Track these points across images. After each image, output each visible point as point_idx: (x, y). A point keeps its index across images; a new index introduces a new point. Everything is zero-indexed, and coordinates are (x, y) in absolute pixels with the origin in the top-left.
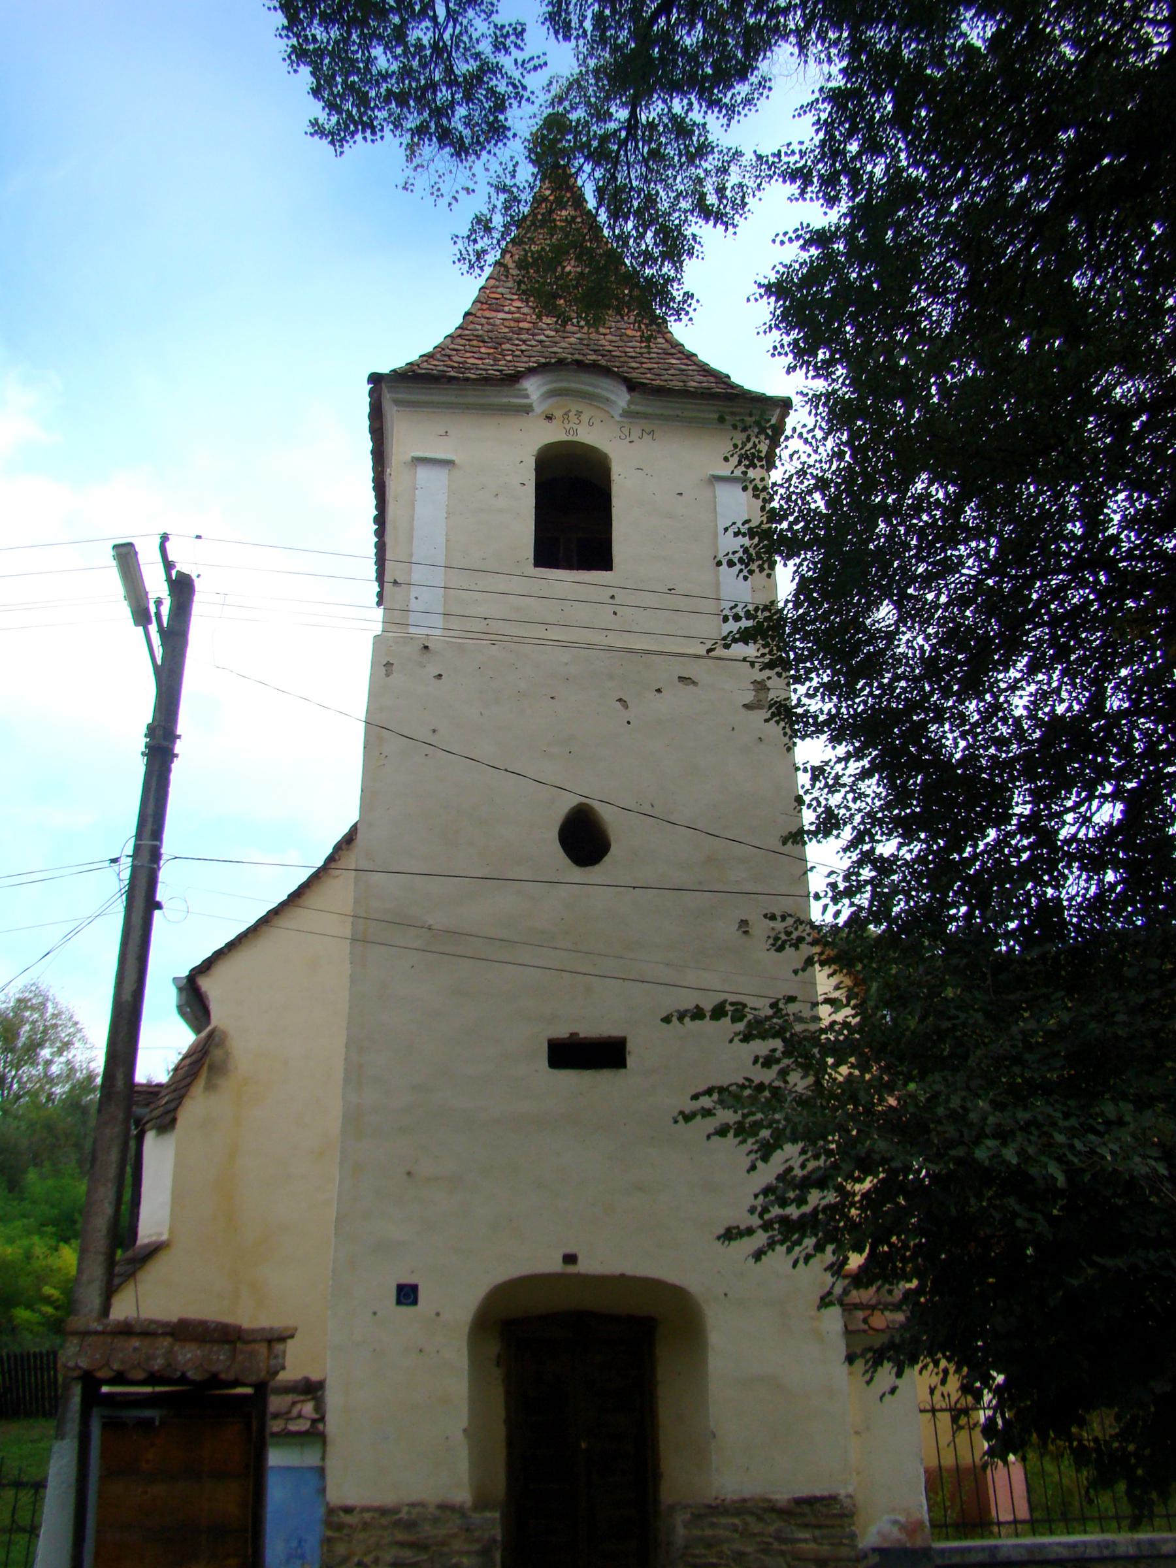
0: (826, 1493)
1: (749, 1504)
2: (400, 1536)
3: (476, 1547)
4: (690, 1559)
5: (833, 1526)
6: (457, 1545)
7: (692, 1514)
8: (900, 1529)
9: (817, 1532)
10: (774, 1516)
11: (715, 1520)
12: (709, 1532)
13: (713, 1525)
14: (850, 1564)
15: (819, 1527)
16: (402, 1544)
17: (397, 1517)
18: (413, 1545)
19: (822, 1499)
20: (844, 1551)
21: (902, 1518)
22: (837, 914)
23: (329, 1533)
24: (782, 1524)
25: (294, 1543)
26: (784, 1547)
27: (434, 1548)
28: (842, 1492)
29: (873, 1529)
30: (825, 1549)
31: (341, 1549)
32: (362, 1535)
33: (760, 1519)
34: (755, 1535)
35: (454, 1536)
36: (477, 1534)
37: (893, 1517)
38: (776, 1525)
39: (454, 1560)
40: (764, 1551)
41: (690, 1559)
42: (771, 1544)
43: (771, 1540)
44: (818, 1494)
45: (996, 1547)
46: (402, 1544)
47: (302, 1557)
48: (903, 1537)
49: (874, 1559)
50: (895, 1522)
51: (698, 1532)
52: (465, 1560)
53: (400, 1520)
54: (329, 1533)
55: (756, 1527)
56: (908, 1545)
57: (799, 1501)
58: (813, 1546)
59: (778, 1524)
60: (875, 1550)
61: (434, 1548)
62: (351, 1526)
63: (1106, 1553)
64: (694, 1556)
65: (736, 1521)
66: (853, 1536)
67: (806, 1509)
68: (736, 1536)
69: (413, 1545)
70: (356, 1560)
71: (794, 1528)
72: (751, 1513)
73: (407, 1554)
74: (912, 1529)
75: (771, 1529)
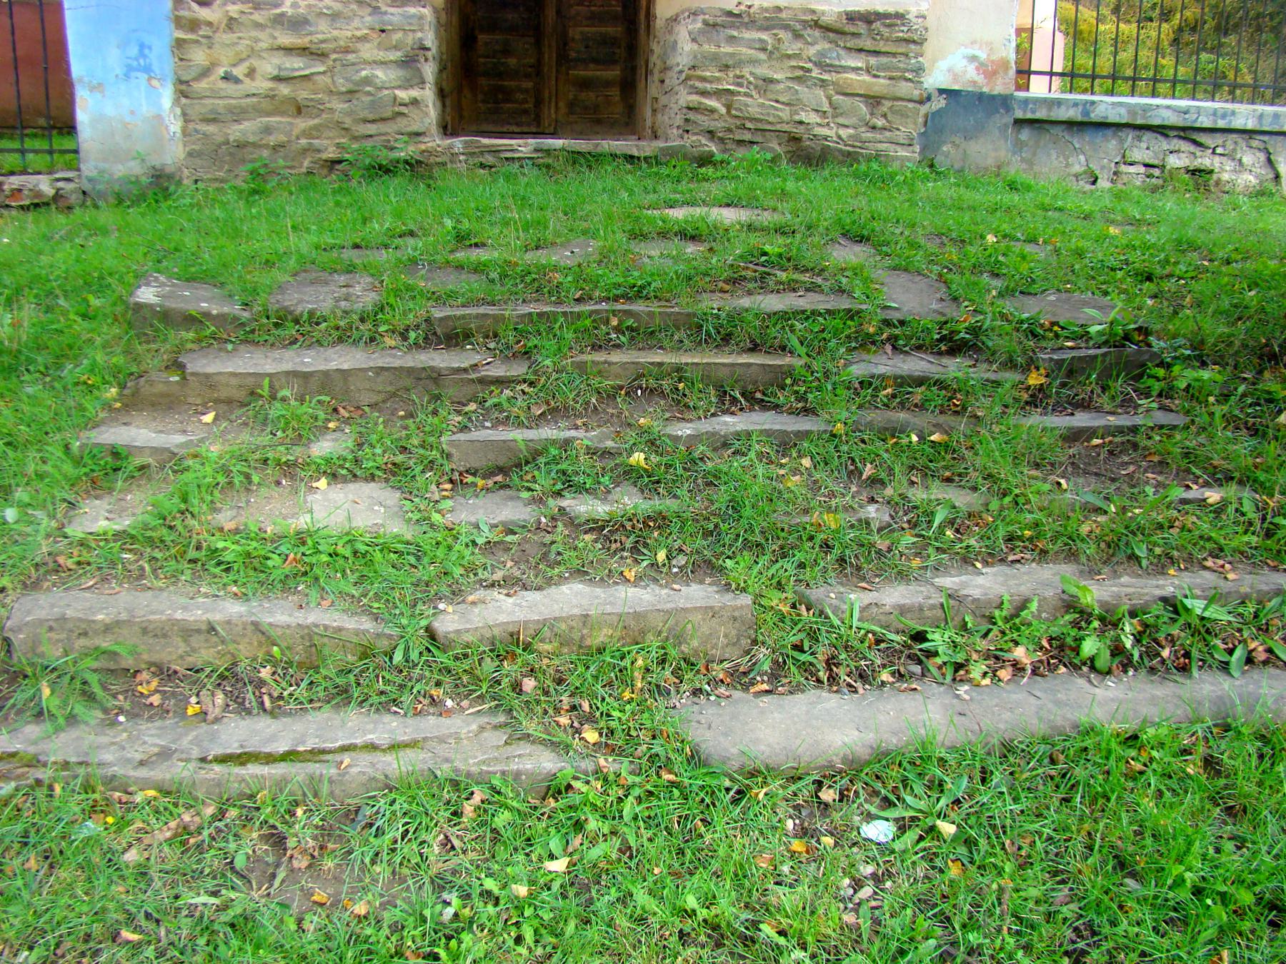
0: (891, 10)
1: (783, 15)
2: (286, 39)
3: (395, 55)
4: (698, 84)
5: (894, 55)
6: (368, 51)
7: (706, 23)
8: (977, 69)
9: (873, 61)
10: (817, 33)
11: (735, 33)
12: (727, 49)
13: (732, 39)
14: (910, 105)
15: (876, 53)
16: (288, 50)
17: (278, 11)
18: (303, 51)
19: (886, 16)
20: (904, 89)
21: (983, 56)
22: (16, 325)
23: (181, 35)
24: (827, 46)
25: (134, 51)
26: (825, 77)
27: (334, 56)
28: (914, 10)
29: (943, 65)
30: (880, 85)
31: (199, 57)
32: (228, 38)
33: (797, 36)
34: (789, 57)
35: (364, 39)
36: (398, 36)
37: (971, 52)
38: (818, 47)
39: (364, 73)
40: (798, 79)
41: (698, 84)
42: (809, 71)
43: (809, 65)
44: (881, 9)
45: (1093, 103)
46: (288, 50)
47: (147, 70)
48: (980, 79)
49: (939, 103)
50: (973, 59)
51: (709, 48)
52: (380, 73)
53: (283, 15)
54: (181, 35)
55: (792, 47)
56: (984, 90)
57: (851, 17)
58: (867, 78)
59: (823, 45)
60: (941, 91)
61: (334, 56)
62: (210, 24)
63: (1221, 124)
64: (704, 79)
65: (764, 36)
66: (919, 70)
67: (861, 28)
68: (763, 56)
69: (303, 51)
70: (221, 71)
71: (842, 52)
72: (786, 27)
73: (296, 64)
74: (990, 71)
75: (812, 51)
